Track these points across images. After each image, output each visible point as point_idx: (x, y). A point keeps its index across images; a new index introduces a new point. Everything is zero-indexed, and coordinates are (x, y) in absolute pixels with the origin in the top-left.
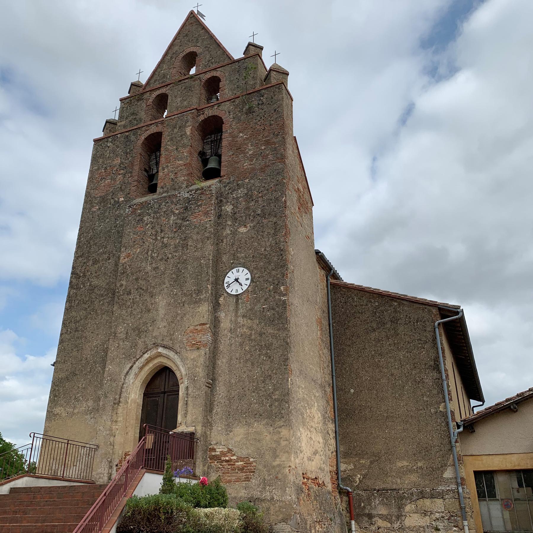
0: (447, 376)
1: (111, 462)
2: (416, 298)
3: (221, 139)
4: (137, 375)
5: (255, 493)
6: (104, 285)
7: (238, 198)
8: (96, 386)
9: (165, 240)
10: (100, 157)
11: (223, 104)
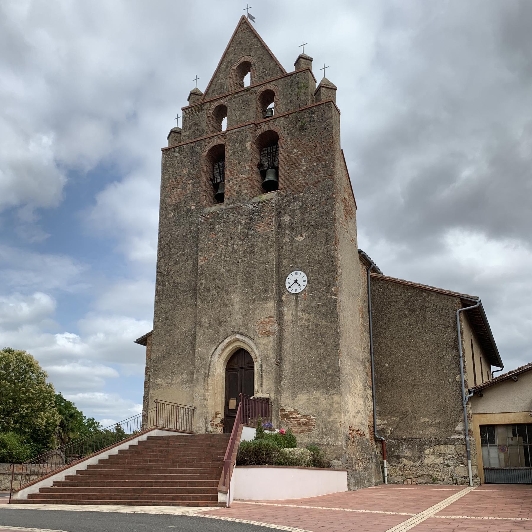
0: (464, 354)
1: (206, 419)
2: (442, 290)
3: (277, 151)
4: (220, 355)
5: (315, 440)
6: (186, 282)
7: (294, 210)
8: (188, 363)
9: (235, 246)
10: (170, 166)
11: (278, 119)
